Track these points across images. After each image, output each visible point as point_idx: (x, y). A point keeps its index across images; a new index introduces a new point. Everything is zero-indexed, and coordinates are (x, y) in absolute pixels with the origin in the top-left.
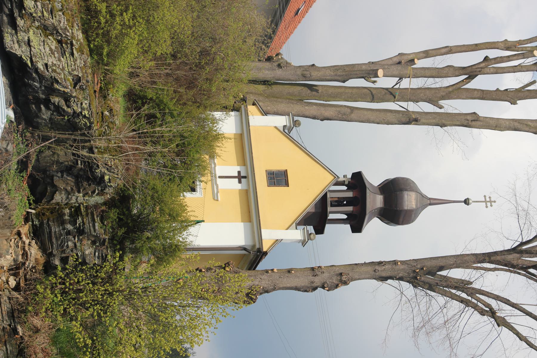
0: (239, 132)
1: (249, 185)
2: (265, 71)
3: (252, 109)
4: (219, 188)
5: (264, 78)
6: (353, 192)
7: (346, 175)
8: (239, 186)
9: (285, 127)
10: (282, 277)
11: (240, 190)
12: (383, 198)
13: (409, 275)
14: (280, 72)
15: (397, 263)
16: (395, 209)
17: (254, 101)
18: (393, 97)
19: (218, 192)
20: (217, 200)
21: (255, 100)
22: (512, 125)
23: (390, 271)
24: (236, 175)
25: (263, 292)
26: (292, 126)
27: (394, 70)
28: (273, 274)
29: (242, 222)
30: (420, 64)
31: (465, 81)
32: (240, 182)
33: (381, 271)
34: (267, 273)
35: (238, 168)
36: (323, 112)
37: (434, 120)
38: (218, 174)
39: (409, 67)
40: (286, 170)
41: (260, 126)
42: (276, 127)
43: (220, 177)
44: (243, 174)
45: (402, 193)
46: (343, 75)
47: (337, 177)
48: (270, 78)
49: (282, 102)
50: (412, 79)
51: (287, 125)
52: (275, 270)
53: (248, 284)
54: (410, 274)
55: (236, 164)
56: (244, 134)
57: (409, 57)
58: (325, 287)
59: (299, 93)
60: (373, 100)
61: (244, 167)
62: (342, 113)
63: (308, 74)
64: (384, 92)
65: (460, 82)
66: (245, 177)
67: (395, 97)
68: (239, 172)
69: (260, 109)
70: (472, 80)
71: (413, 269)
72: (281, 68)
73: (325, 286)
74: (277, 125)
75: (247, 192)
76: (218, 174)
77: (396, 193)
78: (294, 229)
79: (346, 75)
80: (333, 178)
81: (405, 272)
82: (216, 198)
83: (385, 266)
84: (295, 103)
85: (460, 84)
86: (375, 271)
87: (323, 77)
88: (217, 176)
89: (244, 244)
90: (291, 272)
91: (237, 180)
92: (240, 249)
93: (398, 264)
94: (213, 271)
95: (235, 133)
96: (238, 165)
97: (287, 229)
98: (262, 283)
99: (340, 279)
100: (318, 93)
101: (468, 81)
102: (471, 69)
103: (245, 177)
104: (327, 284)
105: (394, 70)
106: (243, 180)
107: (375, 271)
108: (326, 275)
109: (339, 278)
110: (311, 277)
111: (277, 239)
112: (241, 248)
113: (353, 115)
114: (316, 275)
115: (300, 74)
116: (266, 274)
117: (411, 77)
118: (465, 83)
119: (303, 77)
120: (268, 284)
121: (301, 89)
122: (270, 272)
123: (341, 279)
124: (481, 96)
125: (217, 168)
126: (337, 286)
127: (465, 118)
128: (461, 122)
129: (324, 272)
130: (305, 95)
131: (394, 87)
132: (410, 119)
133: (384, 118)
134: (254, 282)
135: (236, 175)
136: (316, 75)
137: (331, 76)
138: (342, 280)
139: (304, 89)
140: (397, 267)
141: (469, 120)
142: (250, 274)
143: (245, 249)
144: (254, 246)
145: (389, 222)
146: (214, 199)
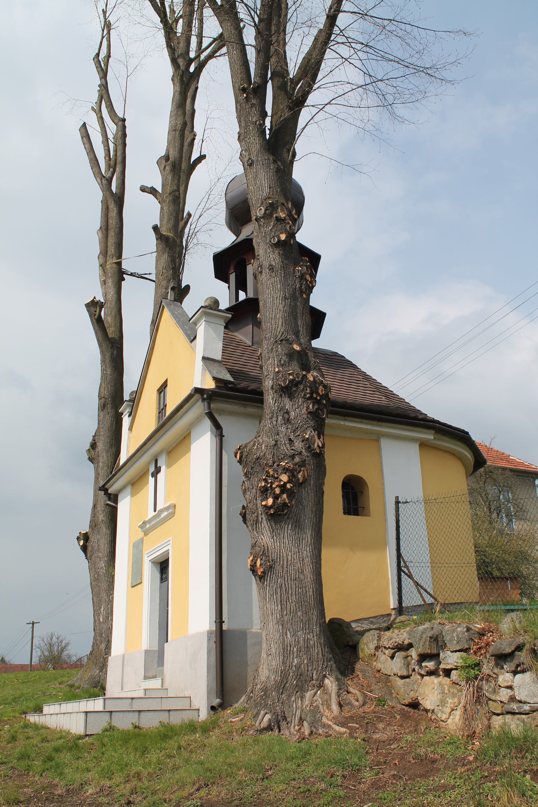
119: (106, 407)
146: (173, 514)
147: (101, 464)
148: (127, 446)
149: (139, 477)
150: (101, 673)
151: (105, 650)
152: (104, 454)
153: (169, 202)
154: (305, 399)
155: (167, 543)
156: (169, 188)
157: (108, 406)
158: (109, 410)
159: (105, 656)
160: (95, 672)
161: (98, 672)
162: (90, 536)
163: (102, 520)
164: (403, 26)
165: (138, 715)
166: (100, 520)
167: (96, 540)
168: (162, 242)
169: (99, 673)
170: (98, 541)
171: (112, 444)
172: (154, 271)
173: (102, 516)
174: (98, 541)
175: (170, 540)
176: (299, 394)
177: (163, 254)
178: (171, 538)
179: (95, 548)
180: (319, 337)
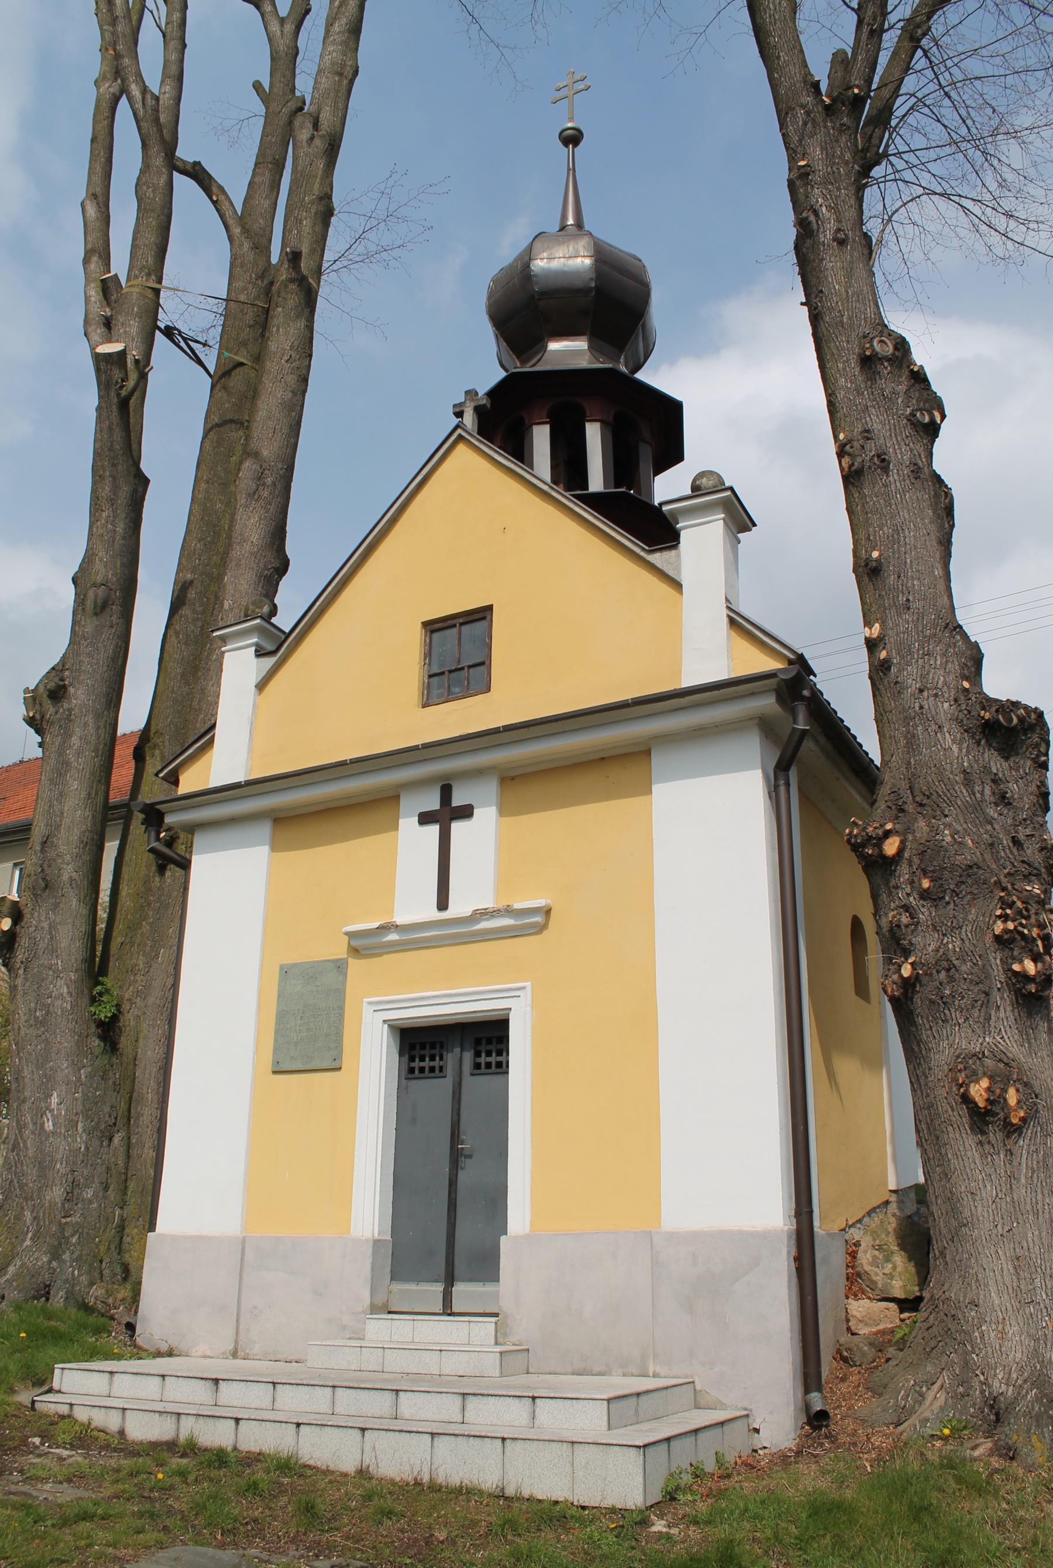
0: (265, 830)
1: (479, 773)
2: (70, 747)
3: (190, 782)
4: (489, 904)
5: (96, 750)
6: (531, 426)
7: (455, 406)
8: (486, 816)
9: (260, 653)
10: (902, 599)
11: (504, 810)
12: (557, 341)
13: (848, 128)
14: (79, 692)
15: (803, 171)
16: (593, 294)
17: (163, 778)
18: (238, 370)
19: (509, 911)
20: (548, 912)
21: (157, 775)
22: (336, 37)
23: (839, 189)
24: (434, 830)
25: (221, 1381)
26: (258, 621)
27: (125, 332)
28: (891, 640)
29: (650, 792)
30: (120, 264)
31: (217, 196)
32: (466, 812)
33: (838, 220)
34: (889, 668)
35: (408, 824)
36: (247, 547)
37: (305, 223)
38: (430, 912)
39: (124, 291)
40: (425, 624)
41: (251, 749)
42: (261, 686)
43: (443, 904)
44: (432, 802)
45: (535, 276)
46: (114, 478)
47: (459, 431)
48: (99, 728)
49: (203, 690)
50: (165, 282)
51: (257, 645)
52: (876, 630)
53: (955, 748)
54: (842, 125)
55: (393, 833)
56: (273, 810)
57: (93, 299)
58: (933, 422)
59: (186, 643)
60: (242, 424)
61: (403, 802)
62: (254, 486)
63: (96, 596)
64: (220, 394)
65: (218, 210)
66: (446, 792)
67: (242, 364)
68: (425, 819)
69: (190, 751)
70: (216, 182)
71: (818, 114)
72: (64, 687)
73: (927, 419)
74: (253, 679)
75: (513, 778)
76: (430, 912)
77: (537, 297)
78: (679, 556)
79: (114, 465)
80: (461, 448)
81: (837, 141)
82: (538, 919)
83: (817, 207)
84: (209, 645)
85: (228, 214)
86: (842, 243)
87: (117, 546)
88: (435, 915)
89: (760, 771)
90: (877, 560)
91: (457, 828)
92: (782, 789)
93: (807, 165)
94: (905, 919)
95: (266, 849)
96: (396, 827)
97: (677, 585)
98: (945, 683)
99: (891, 365)
100: (192, 582)
101: (214, 189)
102: (147, 121)
103: (446, 792)
104: (918, 414)
105: (125, 332)
106: (457, 801)
107: (842, 243)
108: (876, 421)
109: (886, 369)
110: (894, 476)
111: (725, 620)
112: (776, 787)
113: (265, 453)
114: (883, 460)
115: (96, 621)
116: (893, 670)
117: (157, 286)
118: (222, 197)
119: (108, 610)
120: (944, 655)
121: (174, 638)
122: (883, 654)
123: (889, 360)
124: (270, 166)
125: (400, 919)
126: (919, 378)
127: (305, 144)
128: (316, 157)
129: (868, 431)
130: (199, 624)
131: (212, 373)
132: (292, 280)
133: (286, 358)
134: (942, 718)
135: (433, 831)
136: (105, 567)
137: (115, 517)
138: (893, 354)
139: (177, 627)
140: (820, 166)
141: (313, 135)
142: (903, 742)
143: (782, 767)
144: (766, 726)
145: (640, 327)
146: (541, 928)
147: (75, 740)
148: (251, 723)
149: (322, 807)
150: (54, 1264)
151: (63, 1204)
152: (90, 719)
153: (316, 213)
154: (1035, 762)
155: (512, 993)
156: (317, 186)
157: (114, 607)
158: (114, 619)
159: (64, 1221)
160: (37, 1259)
161: (45, 1260)
162: (26, 912)
163: (71, 879)
164: (930, 96)
165: (667, 1448)
166: (65, 877)
167: (45, 925)
168: (300, 291)
169: (50, 1262)
170: (52, 927)
171: (111, 701)
172: (214, 336)
173: (69, 868)
174: (52, 927)
175: (524, 988)
176: (1027, 749)
177: (297, 317)
178: (528, 984)
179: (42, 946)
180: (149, 481)
